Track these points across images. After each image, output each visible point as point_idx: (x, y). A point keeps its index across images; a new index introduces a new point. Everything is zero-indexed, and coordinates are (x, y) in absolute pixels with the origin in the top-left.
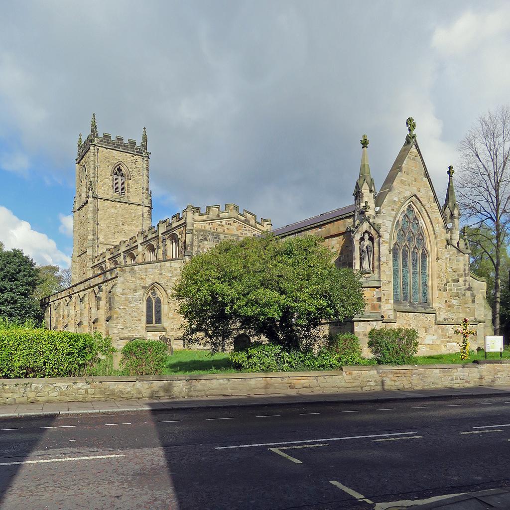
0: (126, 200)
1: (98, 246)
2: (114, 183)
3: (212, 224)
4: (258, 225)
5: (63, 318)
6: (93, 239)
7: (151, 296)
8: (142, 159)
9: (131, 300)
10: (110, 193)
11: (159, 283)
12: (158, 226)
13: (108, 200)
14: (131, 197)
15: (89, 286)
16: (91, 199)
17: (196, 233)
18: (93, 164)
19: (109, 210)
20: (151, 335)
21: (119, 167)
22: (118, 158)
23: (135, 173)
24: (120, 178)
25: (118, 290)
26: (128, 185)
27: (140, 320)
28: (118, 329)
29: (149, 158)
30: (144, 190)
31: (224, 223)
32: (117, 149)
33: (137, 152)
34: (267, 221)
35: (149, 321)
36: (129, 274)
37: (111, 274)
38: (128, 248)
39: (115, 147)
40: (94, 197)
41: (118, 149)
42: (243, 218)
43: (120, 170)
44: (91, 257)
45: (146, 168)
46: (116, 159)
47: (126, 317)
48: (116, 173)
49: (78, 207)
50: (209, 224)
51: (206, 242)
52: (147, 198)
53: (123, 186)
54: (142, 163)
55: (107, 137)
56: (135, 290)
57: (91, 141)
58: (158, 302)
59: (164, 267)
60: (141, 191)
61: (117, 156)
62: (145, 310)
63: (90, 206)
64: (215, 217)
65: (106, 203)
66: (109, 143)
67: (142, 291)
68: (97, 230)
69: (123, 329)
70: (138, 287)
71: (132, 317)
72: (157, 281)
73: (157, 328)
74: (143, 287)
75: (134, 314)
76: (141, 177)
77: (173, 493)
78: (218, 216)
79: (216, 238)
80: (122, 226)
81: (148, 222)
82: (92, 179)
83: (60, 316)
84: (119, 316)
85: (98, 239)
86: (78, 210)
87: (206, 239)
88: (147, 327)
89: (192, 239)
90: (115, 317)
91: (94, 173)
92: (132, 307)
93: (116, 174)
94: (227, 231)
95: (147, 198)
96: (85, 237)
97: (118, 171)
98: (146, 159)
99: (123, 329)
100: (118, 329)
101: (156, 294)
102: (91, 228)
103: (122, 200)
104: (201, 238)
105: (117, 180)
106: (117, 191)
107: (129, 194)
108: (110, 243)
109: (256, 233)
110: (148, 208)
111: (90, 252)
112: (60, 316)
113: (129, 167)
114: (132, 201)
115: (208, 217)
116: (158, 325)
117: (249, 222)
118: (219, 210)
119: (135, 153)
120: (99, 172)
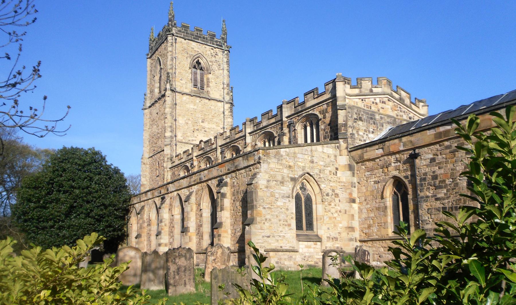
1: (176, 145)
2: (193, 76)
3: (365, 101)
4: (413, 106)
5: (149, 225)
6: (171, 136)
7: (300, 192)
8: (222, 53)
9: (277, 195)
10: (189, 87)
12: (192, 149)
13: (187, 94)
14: (211, 92)
15: (199, 181)
16: (168, 93)
17: (350, 110)
18: (170, 55)
19: (188, 106)
20: (303, 246)
21: (198, 60)
22: (197, 50)
23: (215, 67)
24: (199, 71)
25: (261, 180)
26: (208, 79)
28: (263, 237)
29: (229, 52)
30: (225, 86)
31: (378, 100)
33: (217, 45)
34: (421, 101)
35: (299, 227)
38: (228, 140)
39: (194, 38)
40: (172, 91)
41: (198, 41)
42: (397, 96)
43: (198, 63)
44: (169, 156)
45: (227, 62)
47: (273, 220)
48: (195, 66)
49: (148, 104)
51: (360, 123)
52: (228, 94)
53: (202, 80)
54: (222, 56)
56: (282, 183)
57: (169, 30)
58: (309, 200)
60: (222, 86)
61: (195, 47)
63: (168, 100)
64: (368, 92)
65: (185, 97)
67: (290, 185)
68: (175, 127)
69: (269, 237)
71: (280, 220)
72: (308, 170)
76: (221, 71)
78: (371, 91)
79: (371, 118)
80: (202, 124)
81: (230, 120)
82: (170, 71)
83: (144, 222)
84: (264, 219)
85: (176, 136)
86: (150, 107)
87: (361, 119)
88: (298, 235)
89: (346, 116)
90: (258, 219)
91: (172, 65)
92: (278, 207)
93: (195, 67)
94: (381, 111)
95: (228, 94)
96: (159, 135)
97: (197, 65)
98: (226, 52)
99: (269, 237)
100: (263, 237)
101: (305, 189)
102: (169, 124)
103: (202, 95)
105: (195, 73)
106: (195, 86)
107: (209, 89)
108: (189, 142)
109: (411, 115)
110: (229, 105)
111: (167, 151)
112: (144, 222)
113: (208, 59)
114: (212, 96)
115: (361, 91)
116: (309, 233)
117: (404, 101)
118: (372, 83)
119: (215, 46)
120: (177, 63)
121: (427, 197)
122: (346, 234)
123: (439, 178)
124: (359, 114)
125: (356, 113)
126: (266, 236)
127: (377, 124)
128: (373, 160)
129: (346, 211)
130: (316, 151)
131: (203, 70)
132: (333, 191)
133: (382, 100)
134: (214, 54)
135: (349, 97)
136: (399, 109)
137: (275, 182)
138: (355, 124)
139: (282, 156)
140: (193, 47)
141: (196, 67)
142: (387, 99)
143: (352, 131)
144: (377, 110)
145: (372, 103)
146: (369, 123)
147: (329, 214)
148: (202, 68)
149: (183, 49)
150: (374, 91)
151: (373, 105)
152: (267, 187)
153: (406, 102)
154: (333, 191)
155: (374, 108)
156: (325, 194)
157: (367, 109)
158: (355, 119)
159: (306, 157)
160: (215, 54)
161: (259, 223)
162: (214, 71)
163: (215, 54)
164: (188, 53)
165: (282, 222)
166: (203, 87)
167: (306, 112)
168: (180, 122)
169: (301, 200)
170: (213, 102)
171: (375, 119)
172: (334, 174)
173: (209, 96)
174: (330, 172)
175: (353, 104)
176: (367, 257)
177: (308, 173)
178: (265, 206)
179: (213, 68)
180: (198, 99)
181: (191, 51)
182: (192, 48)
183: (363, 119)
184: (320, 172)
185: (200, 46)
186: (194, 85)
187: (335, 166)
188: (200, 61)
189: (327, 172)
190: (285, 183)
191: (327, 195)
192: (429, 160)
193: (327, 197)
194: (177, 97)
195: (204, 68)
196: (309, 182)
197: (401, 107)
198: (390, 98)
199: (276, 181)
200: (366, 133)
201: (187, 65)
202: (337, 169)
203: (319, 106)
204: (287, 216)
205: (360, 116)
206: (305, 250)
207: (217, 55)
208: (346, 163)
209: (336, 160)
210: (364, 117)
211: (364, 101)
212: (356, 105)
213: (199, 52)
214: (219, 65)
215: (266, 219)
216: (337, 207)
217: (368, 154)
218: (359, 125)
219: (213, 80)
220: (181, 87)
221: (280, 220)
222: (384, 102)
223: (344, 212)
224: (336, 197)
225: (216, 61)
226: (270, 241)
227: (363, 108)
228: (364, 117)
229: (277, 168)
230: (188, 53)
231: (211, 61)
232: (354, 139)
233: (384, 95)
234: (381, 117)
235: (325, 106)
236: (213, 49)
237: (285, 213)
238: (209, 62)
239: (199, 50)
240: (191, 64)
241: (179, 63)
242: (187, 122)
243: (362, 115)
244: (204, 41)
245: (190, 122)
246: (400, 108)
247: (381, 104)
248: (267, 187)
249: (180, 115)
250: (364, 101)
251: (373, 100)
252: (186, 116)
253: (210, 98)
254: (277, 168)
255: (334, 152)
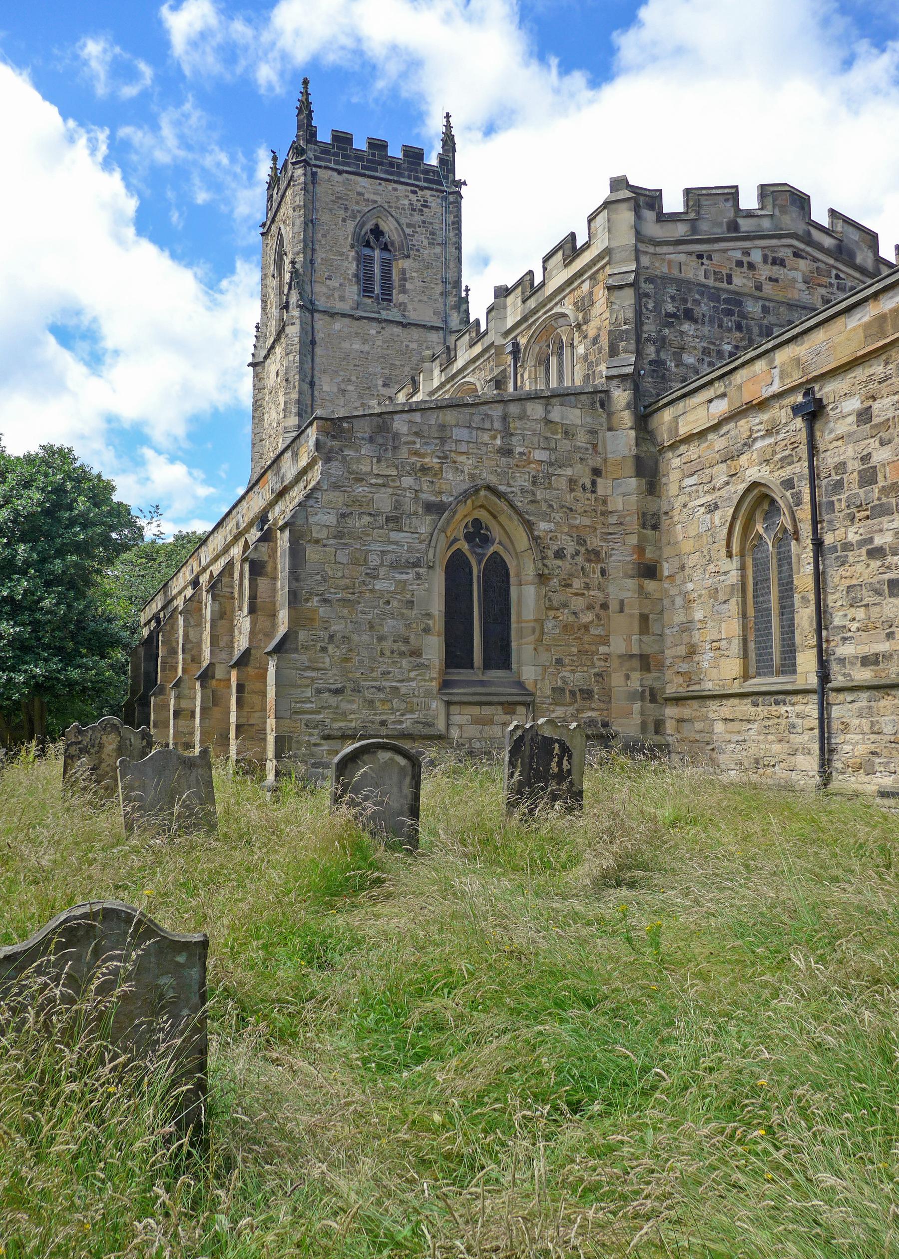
0: (393, 314)
3: (710, 258)
9: (374, 560)
11: (502, 488)
13: (344, 315)
14: (410, 307)
19: (346, 345)
22: (372, 197)
23: (421, 239)
26: (403, 272)
27: (416, 653)
28: (319, 692)
30: (449, 287)
31: (756, 257)
32: (367, 172)
33: (426, 180)
36: (366, 450)
37: (295, 455)
39: (364, 167)
43: (377, 232)
46: (368, 200)
50: (700, 257)
55: (342, 139)
56: (394, 520)
59: (518, 424)
60: (439, 289)
62: (437, 606)
65: (339, 325)
66: (348, 157)
68: (309, 402)
69: (337, 692)
70: (409, 505)
71: (381, 639)
72: (493, 480)
73: (492, 690)
74: (431, 508)
75: (389, 626)
76: (438, 250)
77: (394, 92)
79: (729, 313)
84: (325, 635)
87: (689, 315)
93: (368, 245)
99: (337, 692)
103: (384, 314)
104: (670, 307)
106: (367, 291)
113: (404, 221)
114: (413, 316)
116: (495, 674)
117: (852, 255)
119: (422, 184)
120: (319, 236)
121: (847, 546)
122: (623, 678)
123: (880, 477)
124: (685, 301)
125: (673, 298)
126: (329, 690)
127: (749, 331)
128: (702, 434)
129: (622, 602)
130: (522, 416)
131: (390, 251)
132: (581, 541)
133: (771, 255)
134: (419, 204)
135: (651, 249)
136: (834, 281)
137: (367, 519)
138: (666, 331)
139: (396, 436)
140: (360, 190)
141: (372, 244)
142: (789, 252)
143: (658, 352)
144: (751, 284)
145: (733, 265)
146: (720, 326)
147: (565, 616)
148: (386, 244)
149: (334, 198)
150: (743, 229)
151: (739, 270)
152: (339, 536)
153: (859, 260)
154: (581, 541)
155: (740, 281)
156: (550, 553)
157: (718, 284)
158: (668, 315)
159: (486, 437)
160: (422, 205)
161: (307, 648)
162: (418, 250)
163: (422, 205)
164: (346, 209)
165: (387, 645)
166: (391, 295)
167: (545, 313)
168: (326, 388)
169: (471, 573)
170: (415, 333)
171: (743, 315)
172: (584, 488)
173: (404, 316)
174: (572, 481)
175: (665, 270)
176: (560, 764)
177: (488, 488)
178: (327, 596)
179: (414, 242)
180: (375, 324)
181: (357, 203)
182: (359, 194)
183: (697, 312)
184: (534, 483)
185: (379, 187)
186: (364, 291)
187: (591, 463)
188: (384, 227)
189: (561, 483)
190: (405, 520)
191: (559, 554)
192: (852, 419)
193: (559, 562)
194: (318, 325)
195: (393, 244)
196: (495, 517)
197: (842, 275)
198: (802, 246)
199: (370, 514)
200: (707, 359)
201: (346, 238)
202: (597, 472)
203: (574, 290)
204: (408, 626)
205: (689, 305)
206: (472, 731)
207: (426, 206)
208: (627, 452)
209: (595, 446)
210: (704, 308)
211: (705, 261)
212: (675, 272)
213: (379, 203)
214: (433, 234)
215: (331, 637)
216: (592, 593)
217: (690, 417)
218: (682, 333)
219: (414, 274)
220: (328, 298)
221: (381, 639)
222: (779, 262)
223: (618, 608)
224: (589, 561)
225: (424, 222)
226: (344, 706)
227: (703, 280)
228: (704, 308)
229: (378, 476)
230: (346, 209)
231: (409, 225)
232: (663, 377)
233: (780, 237)
234: (764, 307)
235: (586, 287)
236: (414, 192)
237: (402, 615)
238: (404, 227)
239: (375, 198)
240: (356, 236)
241: (324, 236)
242: (343, 386)
243: (697, 302)
244: (391, 173)
245: (351, 388)
246: (837, 277)
247: (769, 266)
248: (339, 536)
249: (324, 371)
250: (705, 261)
251: (738, 255)
252: (341, 373)
253: (405, 321)
254: (378, 476)
255: (589, 420)
